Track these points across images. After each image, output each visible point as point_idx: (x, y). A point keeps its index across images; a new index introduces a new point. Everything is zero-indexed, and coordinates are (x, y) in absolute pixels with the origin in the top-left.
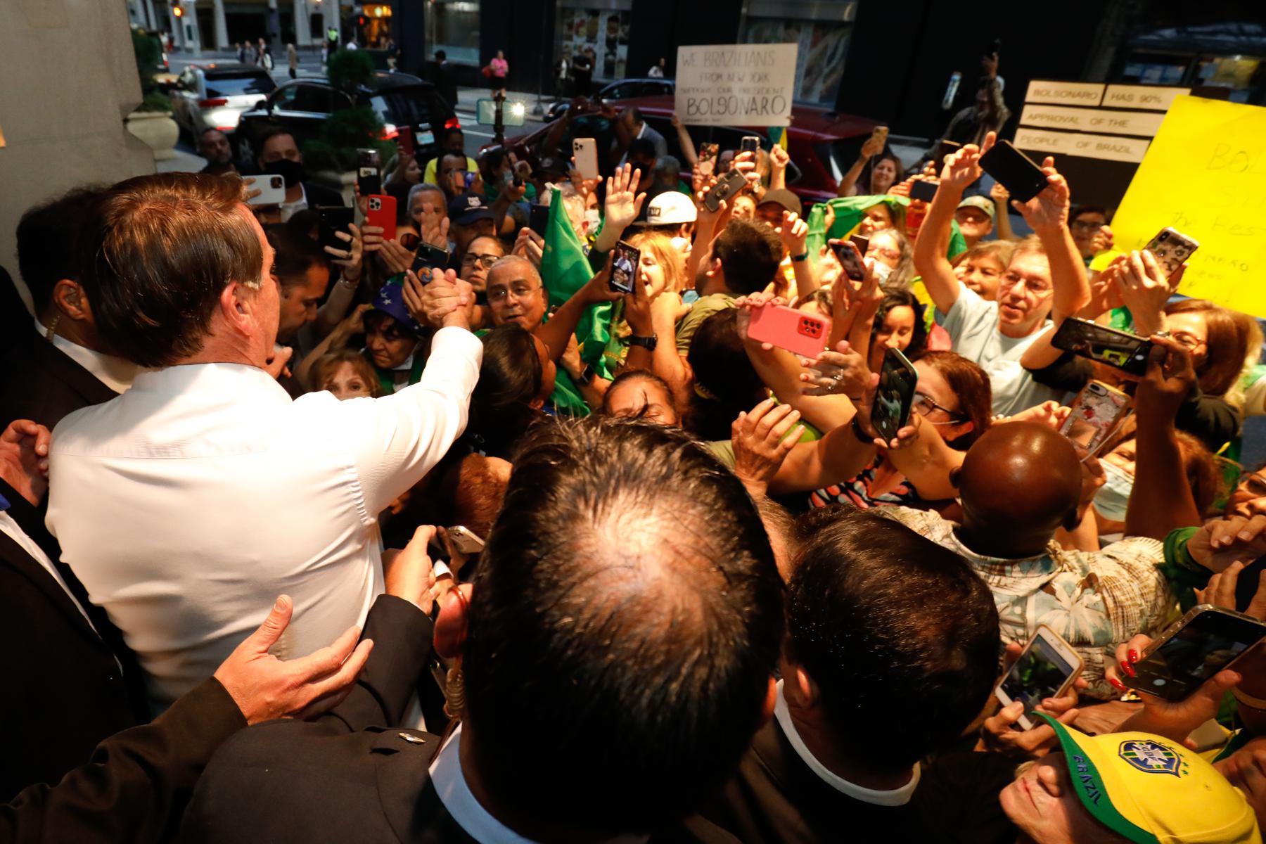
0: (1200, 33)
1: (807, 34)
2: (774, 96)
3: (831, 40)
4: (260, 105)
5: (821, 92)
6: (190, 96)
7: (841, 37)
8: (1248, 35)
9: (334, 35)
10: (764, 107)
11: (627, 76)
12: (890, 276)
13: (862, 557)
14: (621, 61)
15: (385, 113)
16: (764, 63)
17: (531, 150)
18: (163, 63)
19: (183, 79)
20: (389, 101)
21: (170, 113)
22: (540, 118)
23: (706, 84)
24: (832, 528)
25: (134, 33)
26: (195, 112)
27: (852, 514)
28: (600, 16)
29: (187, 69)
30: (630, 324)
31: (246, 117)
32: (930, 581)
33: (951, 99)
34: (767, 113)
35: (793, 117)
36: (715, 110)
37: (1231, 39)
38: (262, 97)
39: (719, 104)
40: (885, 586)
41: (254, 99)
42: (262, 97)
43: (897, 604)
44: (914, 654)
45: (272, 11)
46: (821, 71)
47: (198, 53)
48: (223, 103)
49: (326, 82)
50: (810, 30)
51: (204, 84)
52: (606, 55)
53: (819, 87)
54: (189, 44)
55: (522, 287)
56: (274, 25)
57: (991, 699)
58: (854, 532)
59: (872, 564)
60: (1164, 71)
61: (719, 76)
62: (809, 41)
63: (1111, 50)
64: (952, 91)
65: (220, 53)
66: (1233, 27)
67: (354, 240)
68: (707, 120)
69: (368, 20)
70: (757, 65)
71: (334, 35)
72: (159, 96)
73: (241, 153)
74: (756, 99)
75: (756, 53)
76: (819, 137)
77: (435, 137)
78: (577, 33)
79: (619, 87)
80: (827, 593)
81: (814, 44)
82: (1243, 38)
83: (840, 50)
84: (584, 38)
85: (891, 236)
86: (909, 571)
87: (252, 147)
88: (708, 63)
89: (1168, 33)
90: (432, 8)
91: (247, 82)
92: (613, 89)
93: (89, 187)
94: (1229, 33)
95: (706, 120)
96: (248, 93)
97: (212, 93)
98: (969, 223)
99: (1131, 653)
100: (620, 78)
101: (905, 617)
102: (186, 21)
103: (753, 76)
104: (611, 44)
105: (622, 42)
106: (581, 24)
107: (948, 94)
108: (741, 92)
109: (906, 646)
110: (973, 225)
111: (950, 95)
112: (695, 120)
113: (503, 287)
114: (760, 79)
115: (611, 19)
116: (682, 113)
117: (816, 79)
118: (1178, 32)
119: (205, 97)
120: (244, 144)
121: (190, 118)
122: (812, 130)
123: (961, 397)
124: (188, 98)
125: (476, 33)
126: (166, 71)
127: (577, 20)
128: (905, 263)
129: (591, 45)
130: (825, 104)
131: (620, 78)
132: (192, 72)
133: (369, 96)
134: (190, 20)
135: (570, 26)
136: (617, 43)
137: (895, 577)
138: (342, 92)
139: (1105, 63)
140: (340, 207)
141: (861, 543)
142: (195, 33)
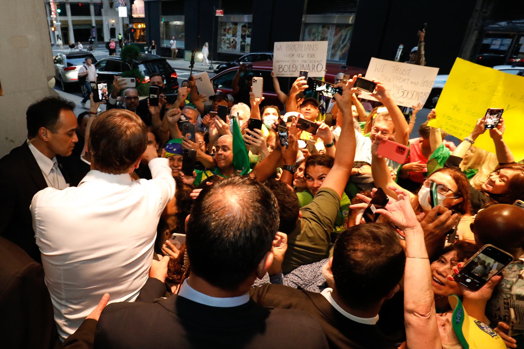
2: (318, 63)
3: (344, 32)
5: (340, 56)
9: (120, 37)
11: (251, 52)
14: (248, 45)
20: (146, 66)
22: (212, 71)
23: (288, 59)
28: (238, 26)
34: (315, 71)
35: (326, 70)
39: (293, 67)
45: (93, 27)
46: (340, 46)
48: (74, 68)
49: (120, 59)
50: (334, 28)
51: (66, 61)
52: (241, 42)
53: (339, 53)
56: (94, 34)
57: (297, 220)
61: (293, 55)
63: (476, 32)
69: (135, 30)
70: (309, 50)
74: (310, 65)
78: (228, 33)
79: (247, 56)
81: (336, 34)
83: (348, 37)
84: (231, 35)
89: (503, 24)
90: (163, 24)
92: (245, 57)
95: (287, 74)
97: (69, 64)
99: (179, 160)
102: (57, 33)
103: (308, 55)
104: (243, 37)
105: (248, 36)
106: (230, 28)
107: (397, 55)
111: (398, 55)
114: (311, 56)
115: (243, 26)
116: (276, 72)
117: (337, 49)
118: (508, 23)
119: (66, 66)
121: (60, 75)
124: (59, 67)
129: (234, 38)
130: (341, 61)
131: (248, 52)
132: (60, 55)
133: (138, 64)
134: (58, 33)
135: (225, 30)
136: (246, 37)
138: (127, 63)
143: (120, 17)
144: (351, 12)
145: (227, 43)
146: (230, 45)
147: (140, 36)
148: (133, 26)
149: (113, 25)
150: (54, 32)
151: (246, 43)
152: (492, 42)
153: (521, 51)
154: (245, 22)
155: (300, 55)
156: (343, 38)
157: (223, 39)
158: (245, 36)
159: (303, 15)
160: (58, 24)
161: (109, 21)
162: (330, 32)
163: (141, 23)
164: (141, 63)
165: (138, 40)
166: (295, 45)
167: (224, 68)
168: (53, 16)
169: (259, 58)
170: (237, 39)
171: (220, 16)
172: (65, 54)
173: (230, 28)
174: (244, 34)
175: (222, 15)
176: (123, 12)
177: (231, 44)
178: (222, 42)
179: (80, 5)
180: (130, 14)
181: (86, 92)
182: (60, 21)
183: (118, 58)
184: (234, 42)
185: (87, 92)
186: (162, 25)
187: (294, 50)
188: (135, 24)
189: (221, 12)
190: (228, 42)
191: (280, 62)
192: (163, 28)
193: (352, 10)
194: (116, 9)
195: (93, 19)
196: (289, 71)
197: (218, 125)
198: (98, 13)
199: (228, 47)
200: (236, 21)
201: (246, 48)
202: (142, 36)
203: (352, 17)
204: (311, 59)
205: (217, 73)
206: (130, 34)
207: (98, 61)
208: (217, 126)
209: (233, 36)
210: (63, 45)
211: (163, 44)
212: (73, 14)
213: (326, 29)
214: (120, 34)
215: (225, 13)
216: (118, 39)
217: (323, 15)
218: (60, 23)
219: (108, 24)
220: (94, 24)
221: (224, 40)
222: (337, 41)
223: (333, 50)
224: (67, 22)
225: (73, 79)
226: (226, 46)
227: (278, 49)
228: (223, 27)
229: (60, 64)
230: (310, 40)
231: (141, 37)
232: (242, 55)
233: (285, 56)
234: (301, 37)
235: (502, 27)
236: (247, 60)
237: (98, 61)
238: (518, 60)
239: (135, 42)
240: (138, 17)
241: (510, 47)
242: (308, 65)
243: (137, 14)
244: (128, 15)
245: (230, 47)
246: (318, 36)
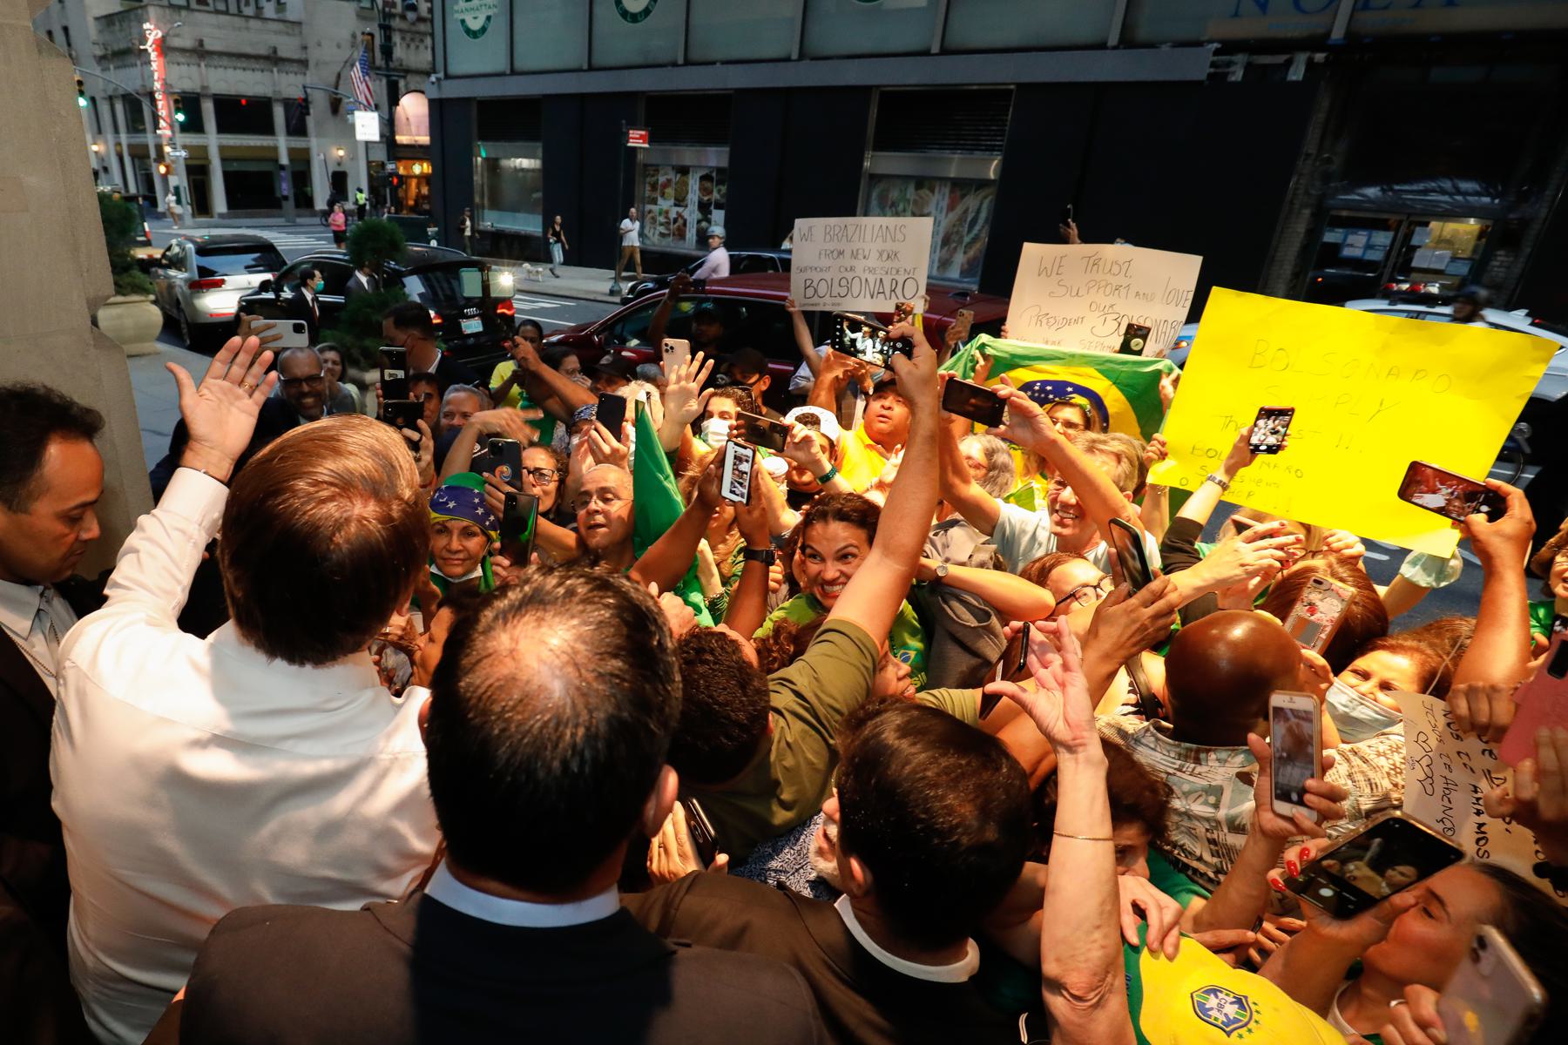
0: (1410, 191)
1: (939, 199)
2: (907, 276)
3: (971, 202)
4: (264, 286)
6: (178, 276)
7: (985, 197)
8: (1465, 194)
13: (904, 745)
17: (600, 340)
18: (145, 234)
19: (168, 253)
20: (427, 282)
21: (152, 297)
22: (617, 299)
24: (878, 719)
25: (103, 199)
26: (183, 293)
27: (897, 705)
29: (174, 242)
30: (743, 534)
32: (963, 762)
37: (1446, 198)
38: (268, 276)
40: (925, 770)
41: (257, 279)
42: (268, 276)
43: (935, 786)
44: (953, 829)
45: (282, 168)
46: (960, 241)
47: (188, 220)
48: (219, 284)
49: (346, 258)
50: (947, 191)
51: (195, 261)
52: (699, 222)
53: (960, 259)
55: (610, 496)
56: (285, 188)
58: (898, 722)
59: (913, 750)
60: (1369, 238)
61: (841, 253)
62: (945, 203)
63: (1307, 212)
65: (215, 220)
66: (1447, 185)
67: (424, 438)
69: (403, 180)
71: (362, 198)
72: (138, 275)
77: (484, 325)
78: (663, 195)
80: (873, 781)
81: (951, 208)
82: (1459, 198)
83: (983, 215)
84: (672, 202)
86: (944, 755)
88: (828, 237)
89: (1372, 192)
91: (249, 258)
93: (14, 385)
94: (1443, 192)
96: (250, 272)
101: (943, 798)
102: (173, 181)
104: (704, 208)
105: (718, 206)
106: (668, 183)
109: (943, 823)
113: (588, 494)
115: (703, 178)
117: (955, 248)
118: (1383, 190)
119: (196, 277)
125: (538, 195)
126: (148, 244)
129: (680, 209)
135: (654, 187)
136: (712, 207)
137: (934, 761)
141: (903, 732)
145: (661, 224)
146: (669, 230)
149: (339, 164)
155: (860, 251)
160: (178, 154)
163: (421, 159)
164: (411, 273)
170: (686, 214)
171: (641, 148)
173: (669, 181)
175: (646, 146)
177: (671, 227)
182: (185, 147)
184: (680, 221)
186: (479, 169)
189: (641, 137)
190: (662, 219)
197: (601, 450)
198: (297, 128)
199: (662, 235)
200: (687, 162)
209: (676, 205)
215: (652, 139)
220: (284, 160)
224: (205, 148)
226: (657, 232)
228: (648, 179)
245: (669, 235)
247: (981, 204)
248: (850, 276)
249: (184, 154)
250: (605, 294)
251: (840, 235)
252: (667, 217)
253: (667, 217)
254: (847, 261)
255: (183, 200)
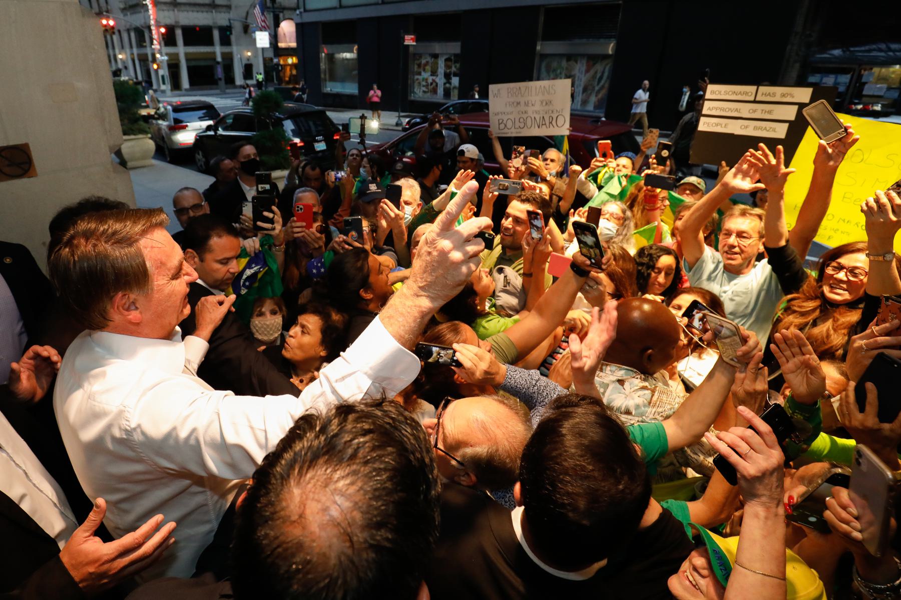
0: (860, 51)
2: (558, 114)
3: (599, 67)
4: (209, 128)
5: (595, 103)
6: (163, 124)
7: (607, 65)
8: (894, 51)
9: (260, 77)
10: (551, 123)
11: (459, 99)
12: (617, 231)
14: (455, 88)
15: (292, 131)
16: (549, 93)
18: (145, 101)
19: (158, 112)
20: (295, 123)
21: (149, 135)
22: (400, 128)
23: (509, 109)
28: (439, 59)
31: (200, 136)
33: (685, 104)
36: (517, 126)
37: (883, 54)
38: (211, 122)
39: (519, 122)
42: (211, 122)
45: (218, 63)
47: (169, 93)
48: (184, 127)
49: (252, 112)
50: (584, 62)
51: (172, 115)
52: (445, 84)
53: (593, 99)
54: (163, 87)
60: (836, 78)
61: (518, 103)
63: (797, 65)
64: (685, 99)
65: (183, 92)
66: (883, 46)
67: (276, 216)
68: (513, 133)
70: (543, 94)
71: (260, 77)
72: (142, 124)
73: (197, 160)
75: (542, 87)
76: (586, 137)
78: (424, 70)
79: (452, 105)
81: (587, 71)
82: (891, 54)
83: (606, 74)
84: (429, 73)
85: (617, 205)
87: (204, 156)
88: (510, 95)
89: (837, 52)
91: (200, 113)
92: (449, 107)
94: (880, 50)
95: (512, 133)
97: (177, 121)
98: (687, 194)
100: (455, 99)
104: (447, 76)
105: (455, 75)
108: (535, 109)
110: (690, 196)
111: (683, 102)
112: (504, 133)
114: (546, 104)
115: (446, 60)
116: (495, 130)
117: (591, 94)
118: (844, 51)
119: (173, 124)
120: (199, 154)
122: (582, 133)
123: (616, 285)
124: (162, 124)
125: (355, 72)
126: (147, 107)
127: (423, 61)
128: (627, 222)
129: (434, 78)
130: (597, 111)
131: (455, 99)
134: (164, 72)
135: (419, 66)
136: (452, 76)
139: (794, 74)
140: (561, 255)
142: (167, 80)
143: (260, 48)
144: (610, 37)
145: (424, 86)
146: (428, 89)
147: (291, 75)
148: (279, 61)
149: (248, 60)
150: (156, 71)
151: (453, 85)
152: (821, 80)
153: (864, 93)
154: (449, 54)
155: (530, 102)
156: (598, 77)
157: (417, 79)
158: (450, 73)
159: (538, 42)
160: (163, 58)
161: (242, 54)
162: (579, 68)
163: (292, 56)
164: (287, 119)
165: (288, 83)
166: (520, 88)
167: (417, 124)
168: (156, 46)
169: (470, 107)
170: (437, 80)
171: (411, 45)
172: (172, 105)
173: (427, 62)
174: (448, 71)
175: (415, 43)
176: (262, 39)
177: (429, 87)
178: (416, 84)
179: (198, 29)
180: (274, 42)
181: (203, 164)
182: (167, 54)
183: (249, 111)
185: (205, 163)
186: (323, 60)
187: (520, 95)
188: (282, 57)
189: (412, 39)
190: (424, 83)
191: (500, 115)
192: (325, 64)
193: (610, 34)
194: (253, 35)
195: (218, 50)
196: (515, 128)
197: (388, 214)
198: (226, 41)
199: (424, 92)
200: (437, 52)
201: (452, 93)
202: (294, 76)
203: (612, 45)
204: (547, 108)
205: (406, 131)
206: (274, 74)
207: (222, 114)
208: (386, 216)
209: (431, 75)
210: (172, 90)
211: (326, 87)
212: (187, 43)
213: (572, 63)
214: (261, 74)
215: (417, 40)
216: (257, 80)
217: (568, 42)
218: (166, 58)
219: (241, 59)
220: (219, 59)
221: (418, 81)
222: (589, 81)
223: (584, 94)
224: (177, 55)
225: (184, 144)
226: (421, 91)
227: (495, 96)
228: (416, 62)
229: (164, 120)
230: (549, 79)
231: (292, 78)
232: (446, 104)
233: (506, 104)
234: (535, 75)
235: (835, 57)
236: (452, 112)
237: (222, 114)
238: (860, 107)
239: (284, 86)
240: (287, 47)
241: (848, 88)
242: (543, 117)
243: (286, 42)
244: (271, 44)
245: (428, 92)
246: (561, 73)
247: (604, 69)
248: (525, 116)
249: (166, 58)
250: (392, 125)
251: (517, 94)
252: (427, 82)
253: (427, 82)
254: (522, 108)
255: (166, 82)
